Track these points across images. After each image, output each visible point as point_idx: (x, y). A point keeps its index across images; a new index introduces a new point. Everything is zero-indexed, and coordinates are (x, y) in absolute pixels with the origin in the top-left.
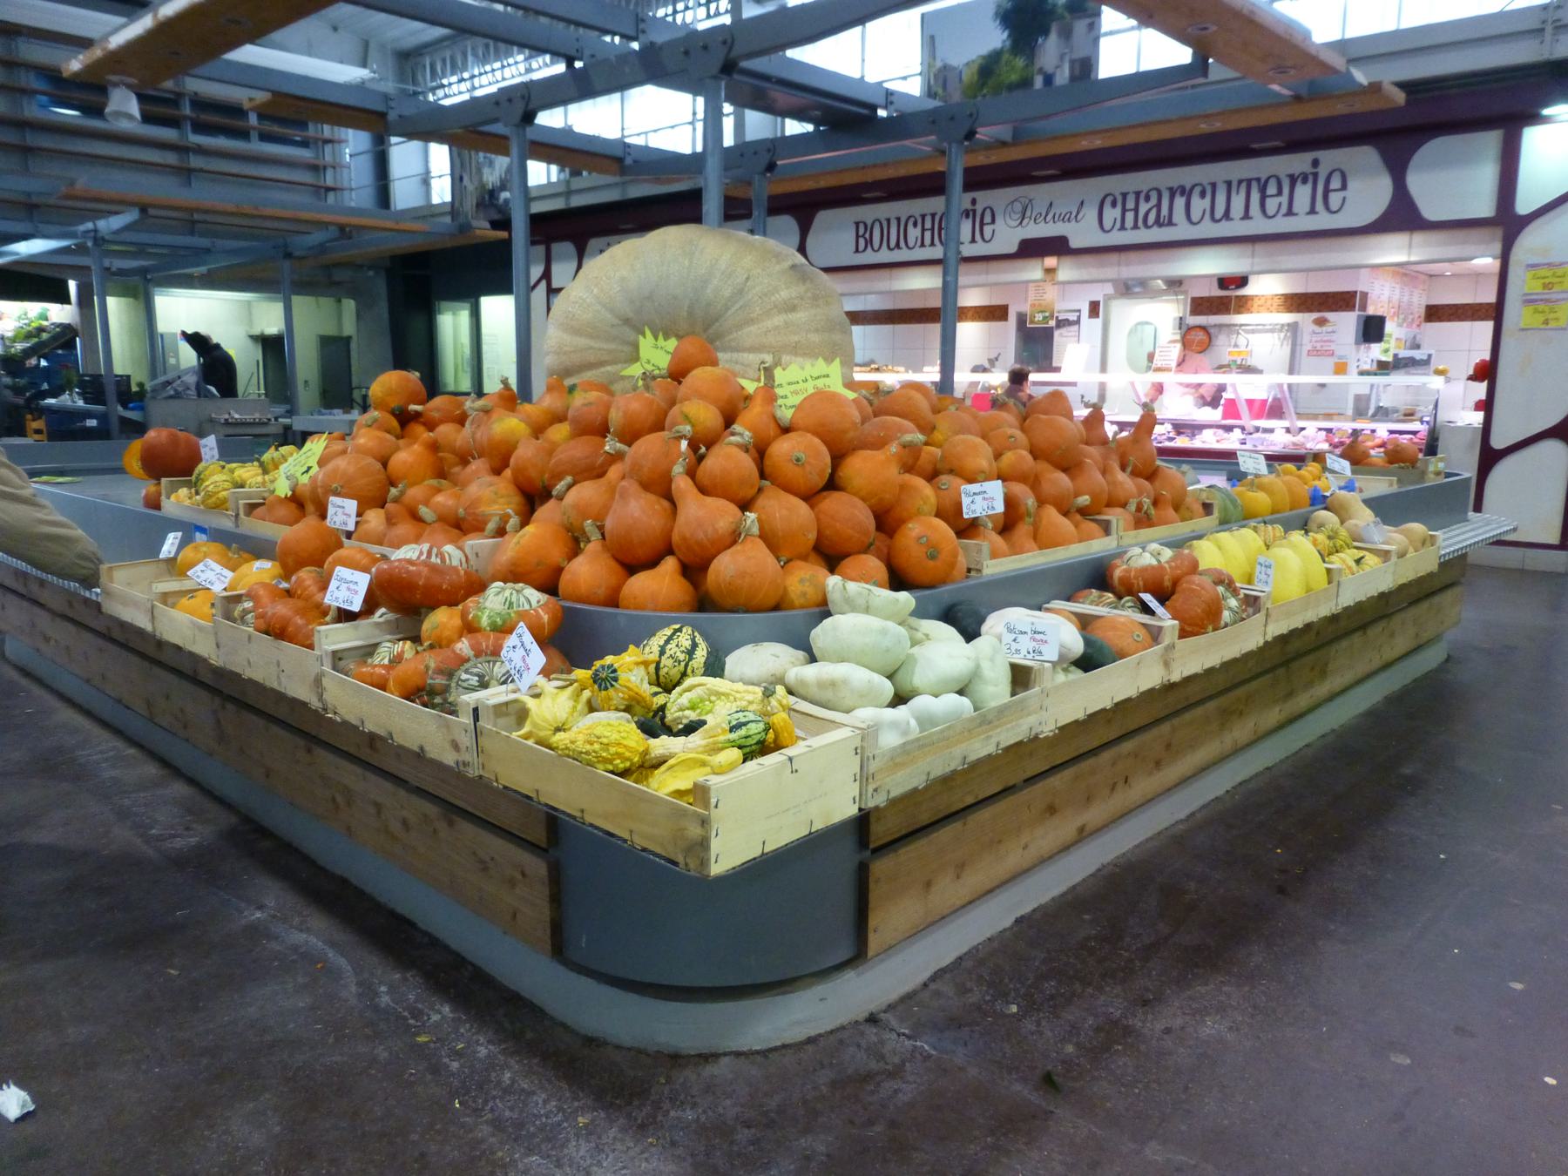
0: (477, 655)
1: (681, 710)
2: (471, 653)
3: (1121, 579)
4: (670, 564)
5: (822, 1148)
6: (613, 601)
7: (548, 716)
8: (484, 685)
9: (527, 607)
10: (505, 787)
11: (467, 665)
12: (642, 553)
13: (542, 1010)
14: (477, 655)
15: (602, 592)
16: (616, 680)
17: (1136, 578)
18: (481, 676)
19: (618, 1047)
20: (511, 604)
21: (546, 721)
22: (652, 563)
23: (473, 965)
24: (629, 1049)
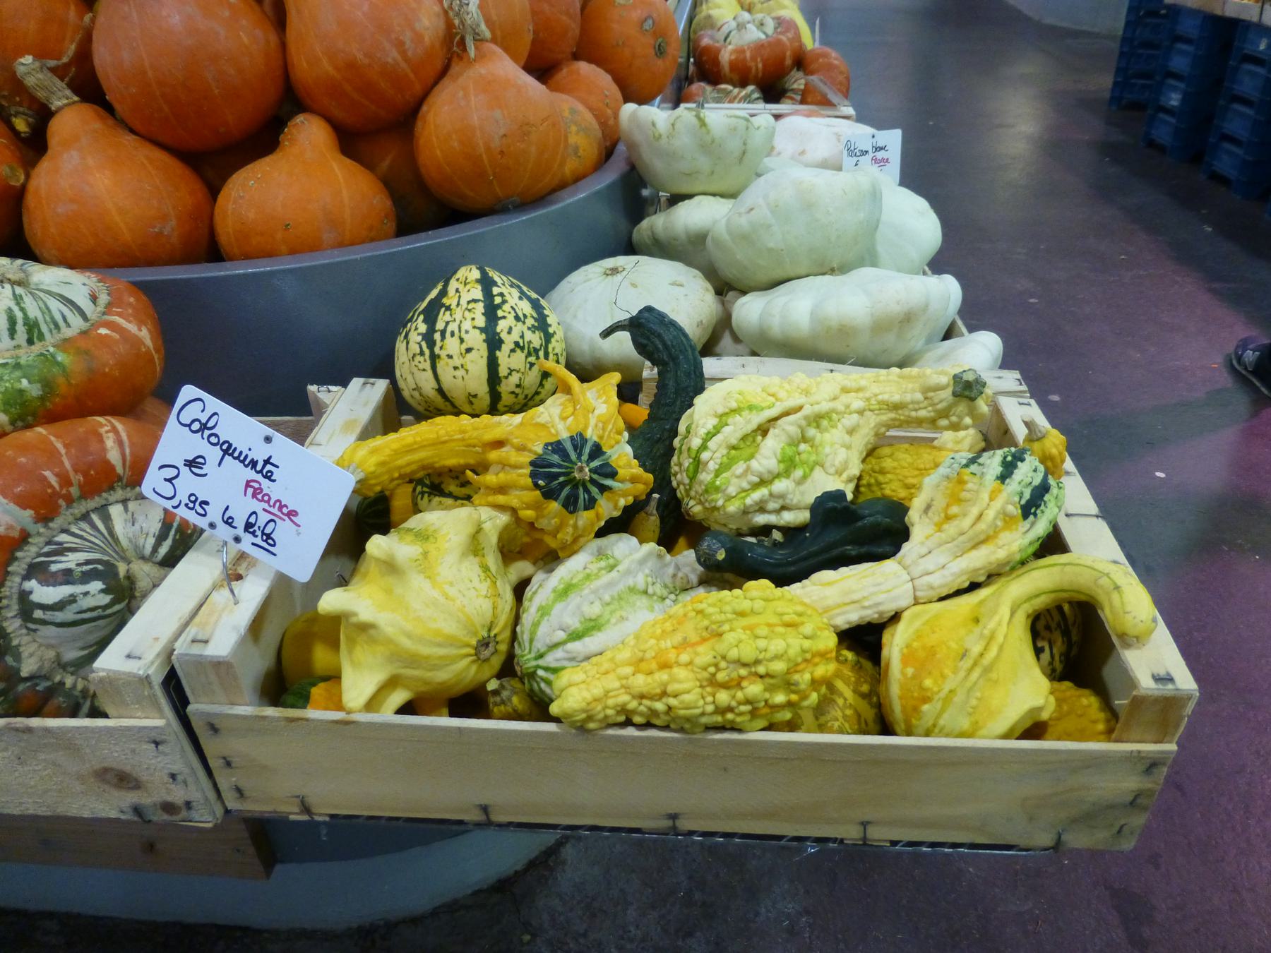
0: (45, 518)
1: (763, 482)
2: (25, 517)
3: (731, 63)
4: (309, 136)
5: (791, 907)
6: (211, 249)
7: (449, 627)
8: (126, 598)
9: (77, 323)
10: (332, 816)
11: (27, 555)
12: (235, 119)
13: (245, 929)
14: (45, 518)
15: (172, 229)
16: (613, 474)
17: (753, 58)
18: (106, 572)
19: (415, 921)
20: (33, 329)
21: (451, 641)
22: (263, 138)
23: (50, 915)
24: (435, 913)
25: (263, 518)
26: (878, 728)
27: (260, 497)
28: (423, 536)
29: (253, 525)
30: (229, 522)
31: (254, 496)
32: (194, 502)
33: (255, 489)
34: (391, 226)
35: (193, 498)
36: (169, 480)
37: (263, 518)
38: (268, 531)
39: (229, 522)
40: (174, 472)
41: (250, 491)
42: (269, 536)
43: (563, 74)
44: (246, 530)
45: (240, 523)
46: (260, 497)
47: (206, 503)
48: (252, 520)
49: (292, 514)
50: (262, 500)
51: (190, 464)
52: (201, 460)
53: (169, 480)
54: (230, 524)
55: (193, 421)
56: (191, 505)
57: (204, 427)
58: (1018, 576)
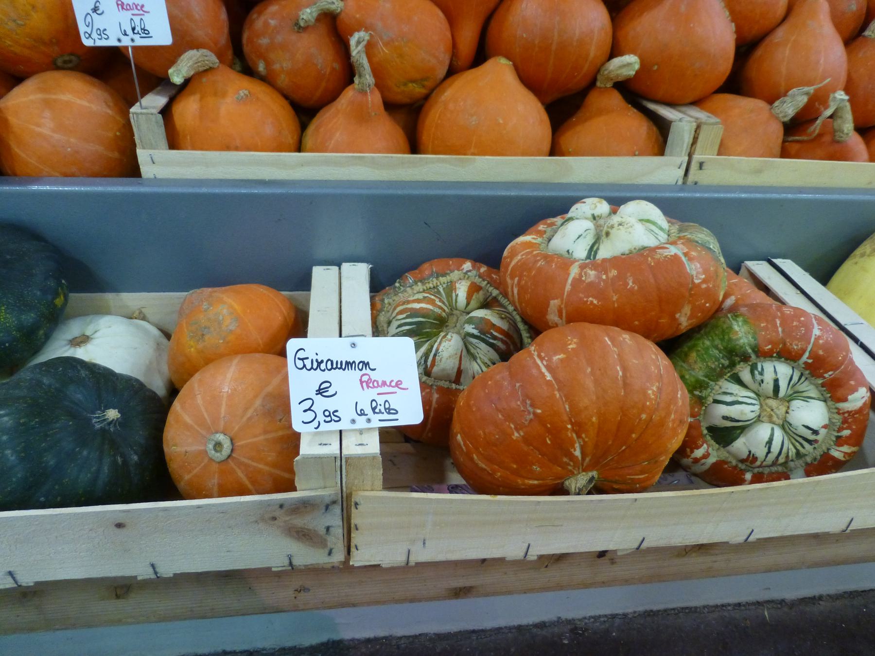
25: (381, 400)
26: (403, 440)
28: (541, 233)
29: (376, 407)
30: (362, 413)
31: (368, 387)
32: (330, 415)
33: (367, 382)
34: (777, 149)
35: (327, 413)
36: (309, 409)
39: (362, 413)
40: (309, 402)
41: (364, 384)
43: (435, 119)
44: (375, 413)
45: (368, 410)
46: (371, 385)
47: (336, 411)
48: (374, 404)
49: (398, 384)
50: (374, 387)
51: (320, 392)
52: (327, 385)
53: (309, 409)
54: (364, 414)
55: (324, 370)
57: (319, 363)
58: (801, 190)
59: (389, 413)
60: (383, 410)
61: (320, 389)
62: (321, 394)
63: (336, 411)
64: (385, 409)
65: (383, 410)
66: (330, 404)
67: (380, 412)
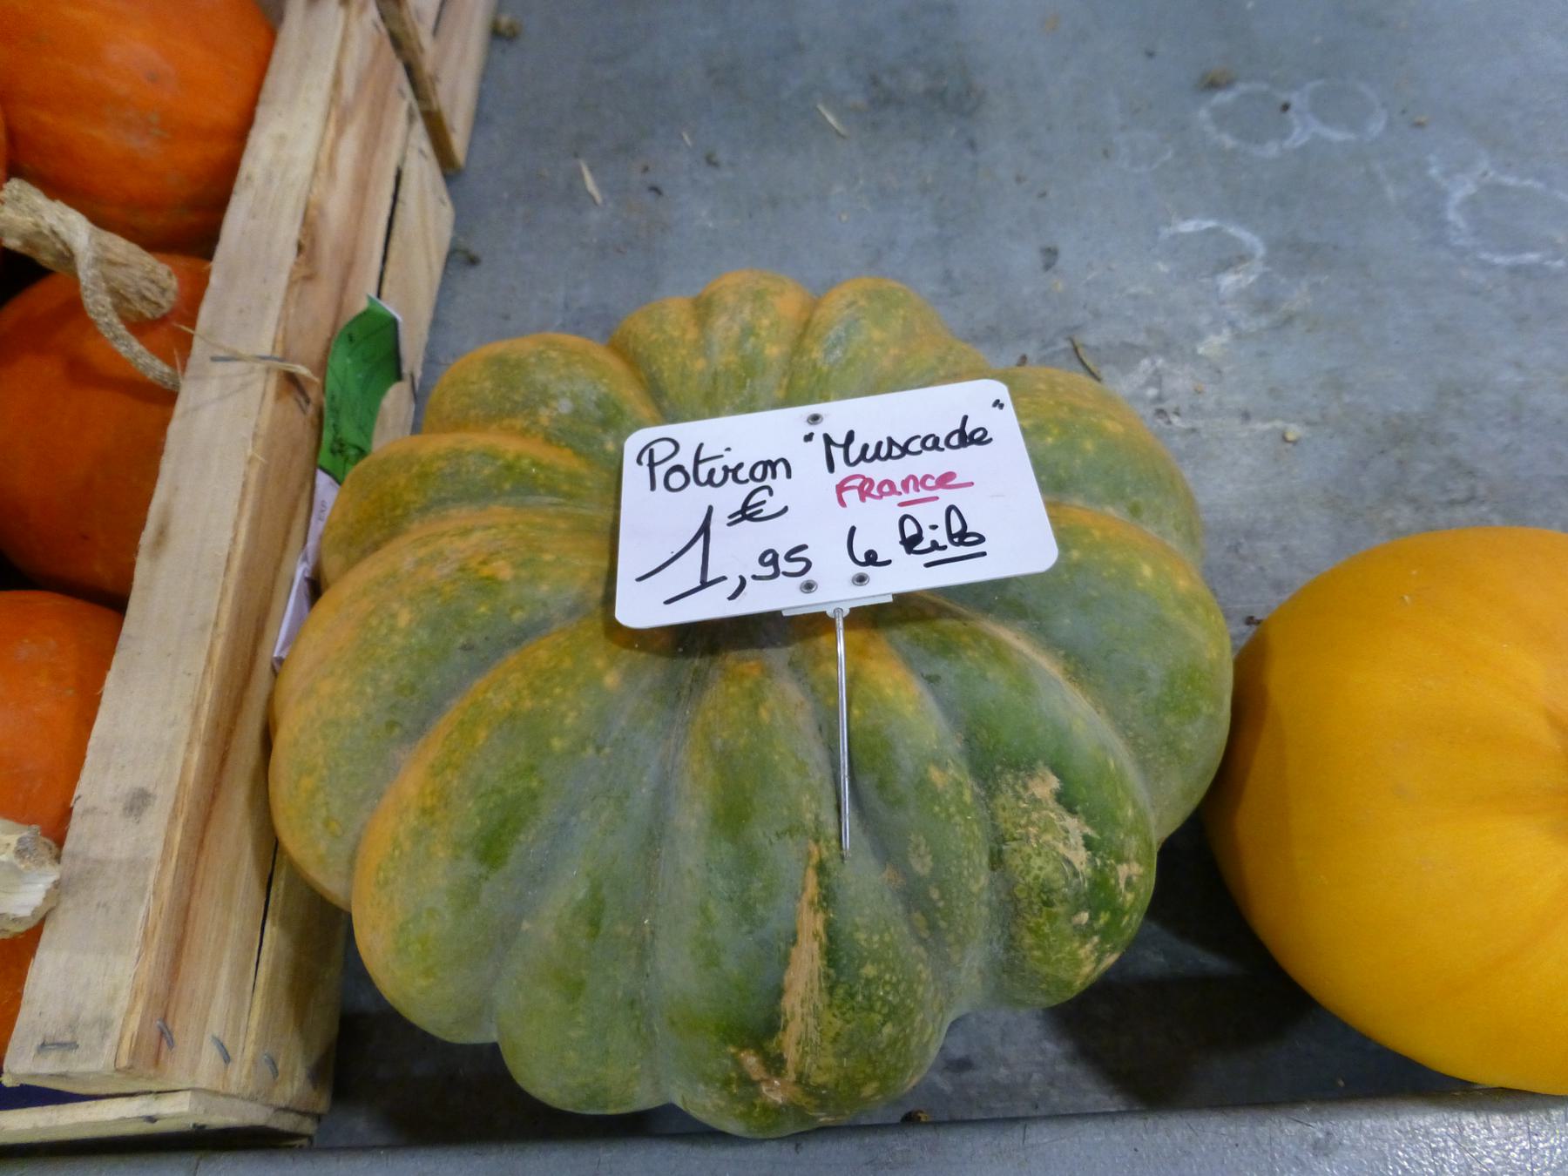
25: (930, 515)
27: (875, 492)
29: (918, 538)
32: (774, 562)
35: (769, 558)
37: (930, 515)
38: (956, 527)
42: (963, 534)
47: (803, 547)
48: (911, 530)
50: (882, 495)
56: (770, 570)
59: (962, 543)
60: (943, 539)
61: (745, 506)
62: (751, 518)
63: (803, 547)
64: (951, 536)
65: (943, 539)
66: (779, 536)
67: (935, 546)
